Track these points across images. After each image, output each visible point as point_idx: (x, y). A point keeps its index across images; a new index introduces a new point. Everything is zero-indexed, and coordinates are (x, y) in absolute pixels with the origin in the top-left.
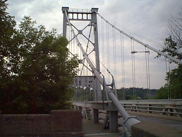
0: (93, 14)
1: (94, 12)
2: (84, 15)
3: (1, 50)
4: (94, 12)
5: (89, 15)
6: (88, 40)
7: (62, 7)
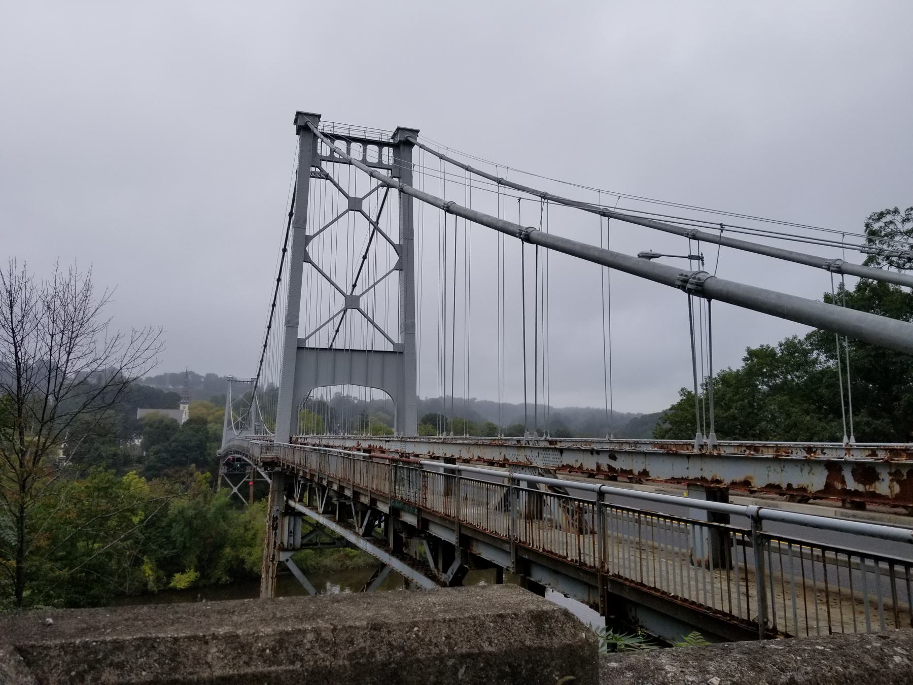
0: (402, 147)
1: (404, 142)
2: (369, 147)
3: (715, 680)
4: (404, 142)
5: (385, 149)
6: (372, 227)
7: (298, 114)
